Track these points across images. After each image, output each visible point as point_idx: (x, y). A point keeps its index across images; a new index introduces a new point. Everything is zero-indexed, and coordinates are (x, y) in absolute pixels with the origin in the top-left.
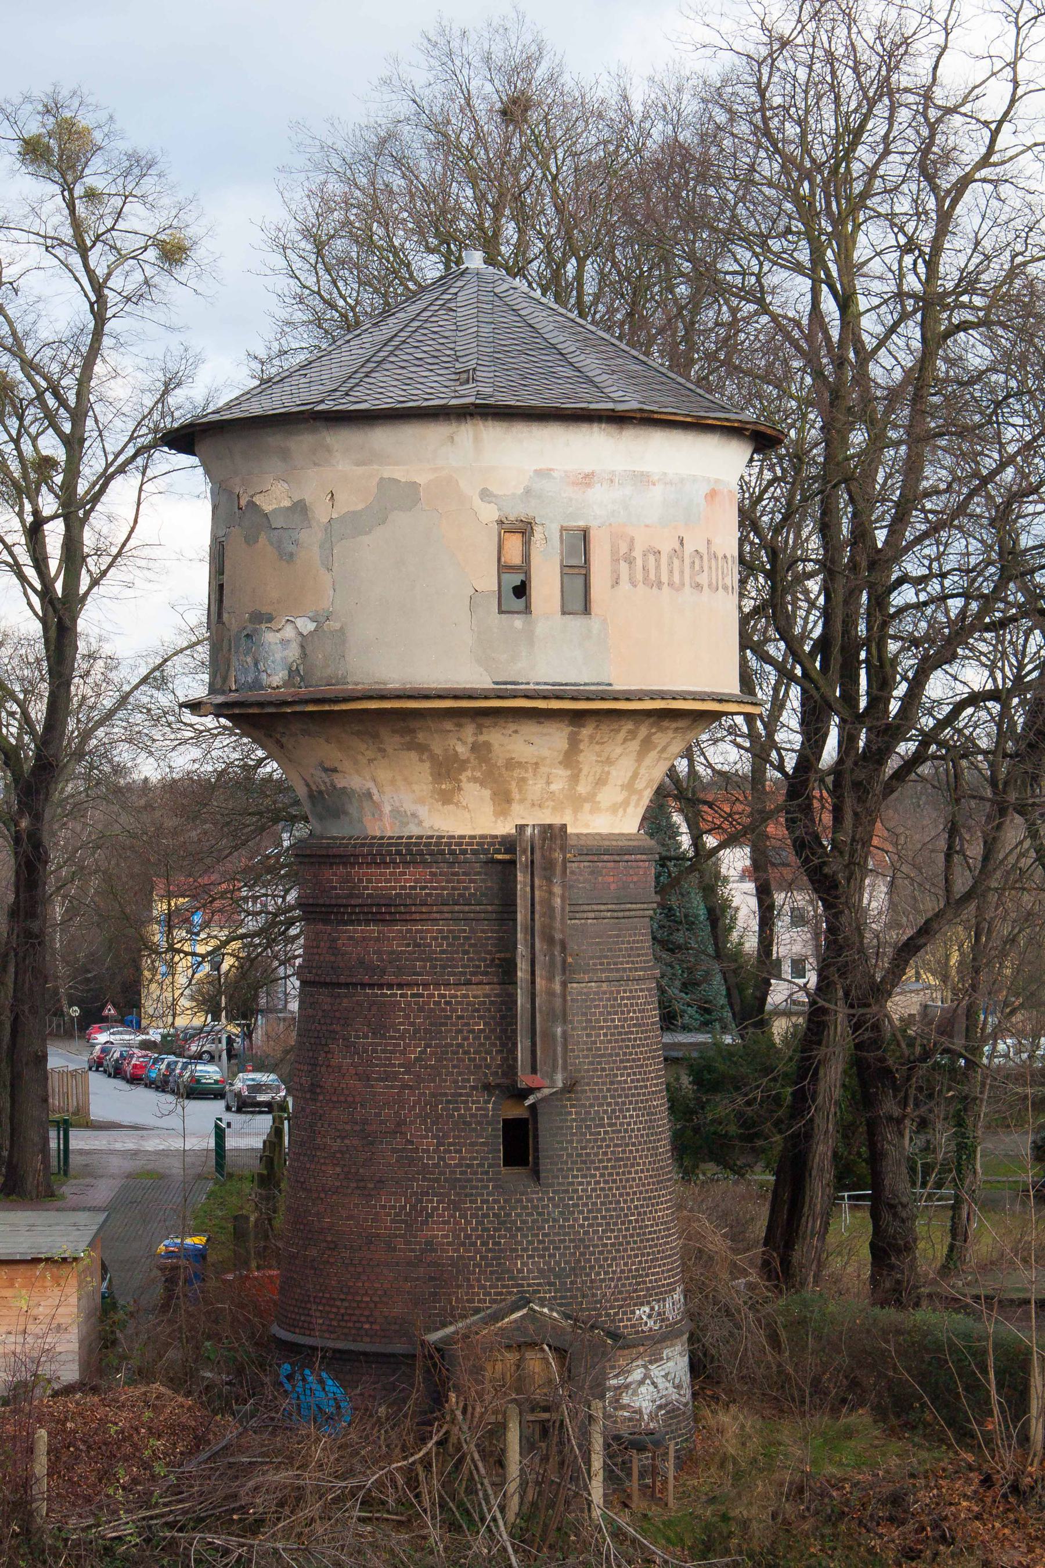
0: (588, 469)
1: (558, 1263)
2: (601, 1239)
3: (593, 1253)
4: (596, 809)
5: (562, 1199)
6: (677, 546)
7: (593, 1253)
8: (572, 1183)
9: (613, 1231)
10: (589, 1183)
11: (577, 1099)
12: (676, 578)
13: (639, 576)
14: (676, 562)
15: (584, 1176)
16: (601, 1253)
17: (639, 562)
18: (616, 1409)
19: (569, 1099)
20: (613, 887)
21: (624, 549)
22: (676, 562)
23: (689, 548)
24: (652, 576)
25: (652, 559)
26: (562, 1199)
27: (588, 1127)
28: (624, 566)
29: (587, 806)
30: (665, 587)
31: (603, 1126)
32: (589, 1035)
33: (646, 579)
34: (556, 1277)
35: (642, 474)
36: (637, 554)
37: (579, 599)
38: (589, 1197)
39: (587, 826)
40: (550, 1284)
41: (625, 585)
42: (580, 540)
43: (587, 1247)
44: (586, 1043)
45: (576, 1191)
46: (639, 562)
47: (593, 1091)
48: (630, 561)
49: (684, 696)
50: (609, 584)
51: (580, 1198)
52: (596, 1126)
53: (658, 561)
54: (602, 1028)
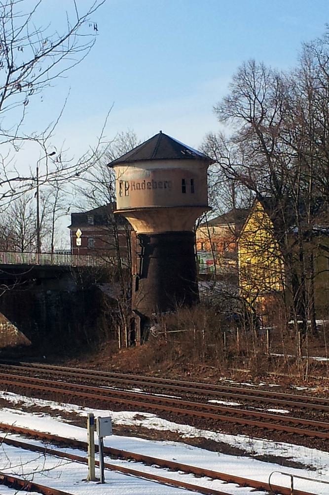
12: (143, 187)
13: (136, 188)
14: (143, 185)
17: (136, 186)
36: (135, 184)
48: (134, 186)
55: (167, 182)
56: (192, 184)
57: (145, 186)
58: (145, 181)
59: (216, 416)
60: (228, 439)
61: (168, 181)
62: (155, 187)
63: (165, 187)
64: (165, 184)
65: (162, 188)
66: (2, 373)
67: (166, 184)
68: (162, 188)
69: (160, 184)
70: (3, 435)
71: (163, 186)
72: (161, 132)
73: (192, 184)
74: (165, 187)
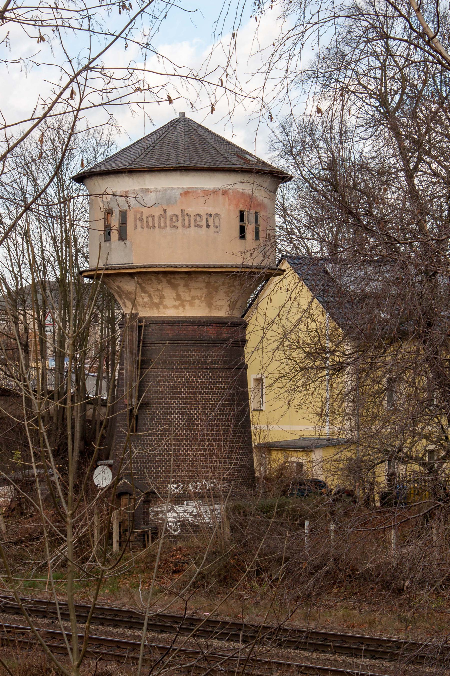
0: (127, 190)
1: (140, 466)
2: (155, 458)
3: (151, 463)
4: (165, 307)
5: (143, 444)
6: (163, 213)
7: (151, 463)
8: (146, 439)
9: (160, 456)
10: (152, 439)
11: (151, 409)
12: (162, 224)
13: (145, 225)
14: (162, 219)
15: (151, 436)
16: (155, 463)
17: (145, 220)
18: (155, 519)
19: (148, 409)
20: (170, 335)
21: (138, 216)
22: (162, 219)
23: (169, 213)
24: (151, 224)
25: (150, 219)
26: (143, 444)
27: (154, 419)
28: (139, 222)
29: (161, 307)
30: (157, 228)
31: (160, 419)
32: (157, 387)
33: (148, 226)
34: (139, 471)
35: (146, 189)
36: (144, 218)
37: (123, 237)
38: (152, 444)
39: (165, 314)
40: (138, 473)
41: (139, 229)
42: (124, 216)
43: (150, 461)
44: (155, 390)
45: (147, 441)
46: (145, 220)
47: (157, 407)
48: (141, 220)
49: (151, 266)
50: (133, 228)
51: (149, 444)
52: (157, 419)
53: (190, 220)
54: (163, 385)
55: (211, 215)
56: (242, 230)
57: (165, 222)
58: (165, 211)
59: (31, 253)
60: (110, 393)
61: (213, 214)
62: (187, 224)
63: (208, 226)
64: (207, 220)
65: (201, 227)
66: (3, 470)
67: (209, 218)
68: (201, 227)
69: (198, 219)
70: (228, 2)
71: (204, 223)
72: (184, 114)
73: (242, 230)
74: (208, 226)
